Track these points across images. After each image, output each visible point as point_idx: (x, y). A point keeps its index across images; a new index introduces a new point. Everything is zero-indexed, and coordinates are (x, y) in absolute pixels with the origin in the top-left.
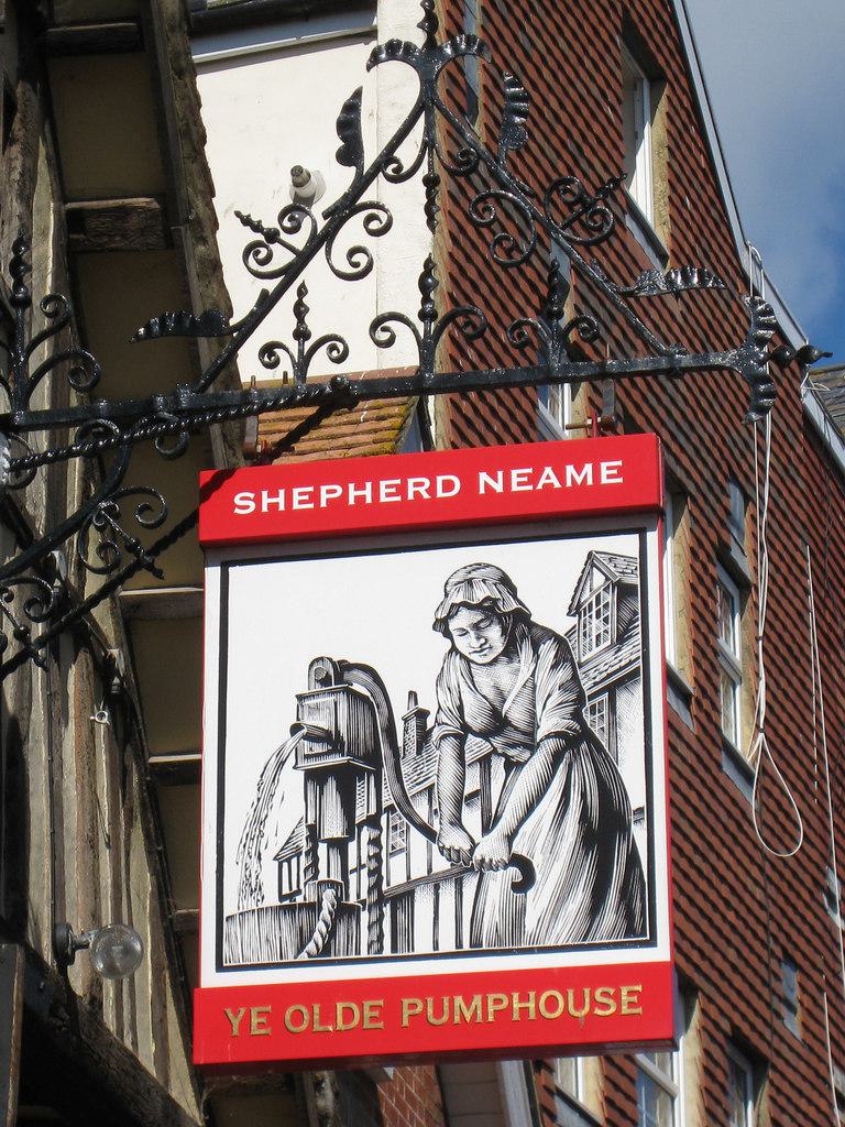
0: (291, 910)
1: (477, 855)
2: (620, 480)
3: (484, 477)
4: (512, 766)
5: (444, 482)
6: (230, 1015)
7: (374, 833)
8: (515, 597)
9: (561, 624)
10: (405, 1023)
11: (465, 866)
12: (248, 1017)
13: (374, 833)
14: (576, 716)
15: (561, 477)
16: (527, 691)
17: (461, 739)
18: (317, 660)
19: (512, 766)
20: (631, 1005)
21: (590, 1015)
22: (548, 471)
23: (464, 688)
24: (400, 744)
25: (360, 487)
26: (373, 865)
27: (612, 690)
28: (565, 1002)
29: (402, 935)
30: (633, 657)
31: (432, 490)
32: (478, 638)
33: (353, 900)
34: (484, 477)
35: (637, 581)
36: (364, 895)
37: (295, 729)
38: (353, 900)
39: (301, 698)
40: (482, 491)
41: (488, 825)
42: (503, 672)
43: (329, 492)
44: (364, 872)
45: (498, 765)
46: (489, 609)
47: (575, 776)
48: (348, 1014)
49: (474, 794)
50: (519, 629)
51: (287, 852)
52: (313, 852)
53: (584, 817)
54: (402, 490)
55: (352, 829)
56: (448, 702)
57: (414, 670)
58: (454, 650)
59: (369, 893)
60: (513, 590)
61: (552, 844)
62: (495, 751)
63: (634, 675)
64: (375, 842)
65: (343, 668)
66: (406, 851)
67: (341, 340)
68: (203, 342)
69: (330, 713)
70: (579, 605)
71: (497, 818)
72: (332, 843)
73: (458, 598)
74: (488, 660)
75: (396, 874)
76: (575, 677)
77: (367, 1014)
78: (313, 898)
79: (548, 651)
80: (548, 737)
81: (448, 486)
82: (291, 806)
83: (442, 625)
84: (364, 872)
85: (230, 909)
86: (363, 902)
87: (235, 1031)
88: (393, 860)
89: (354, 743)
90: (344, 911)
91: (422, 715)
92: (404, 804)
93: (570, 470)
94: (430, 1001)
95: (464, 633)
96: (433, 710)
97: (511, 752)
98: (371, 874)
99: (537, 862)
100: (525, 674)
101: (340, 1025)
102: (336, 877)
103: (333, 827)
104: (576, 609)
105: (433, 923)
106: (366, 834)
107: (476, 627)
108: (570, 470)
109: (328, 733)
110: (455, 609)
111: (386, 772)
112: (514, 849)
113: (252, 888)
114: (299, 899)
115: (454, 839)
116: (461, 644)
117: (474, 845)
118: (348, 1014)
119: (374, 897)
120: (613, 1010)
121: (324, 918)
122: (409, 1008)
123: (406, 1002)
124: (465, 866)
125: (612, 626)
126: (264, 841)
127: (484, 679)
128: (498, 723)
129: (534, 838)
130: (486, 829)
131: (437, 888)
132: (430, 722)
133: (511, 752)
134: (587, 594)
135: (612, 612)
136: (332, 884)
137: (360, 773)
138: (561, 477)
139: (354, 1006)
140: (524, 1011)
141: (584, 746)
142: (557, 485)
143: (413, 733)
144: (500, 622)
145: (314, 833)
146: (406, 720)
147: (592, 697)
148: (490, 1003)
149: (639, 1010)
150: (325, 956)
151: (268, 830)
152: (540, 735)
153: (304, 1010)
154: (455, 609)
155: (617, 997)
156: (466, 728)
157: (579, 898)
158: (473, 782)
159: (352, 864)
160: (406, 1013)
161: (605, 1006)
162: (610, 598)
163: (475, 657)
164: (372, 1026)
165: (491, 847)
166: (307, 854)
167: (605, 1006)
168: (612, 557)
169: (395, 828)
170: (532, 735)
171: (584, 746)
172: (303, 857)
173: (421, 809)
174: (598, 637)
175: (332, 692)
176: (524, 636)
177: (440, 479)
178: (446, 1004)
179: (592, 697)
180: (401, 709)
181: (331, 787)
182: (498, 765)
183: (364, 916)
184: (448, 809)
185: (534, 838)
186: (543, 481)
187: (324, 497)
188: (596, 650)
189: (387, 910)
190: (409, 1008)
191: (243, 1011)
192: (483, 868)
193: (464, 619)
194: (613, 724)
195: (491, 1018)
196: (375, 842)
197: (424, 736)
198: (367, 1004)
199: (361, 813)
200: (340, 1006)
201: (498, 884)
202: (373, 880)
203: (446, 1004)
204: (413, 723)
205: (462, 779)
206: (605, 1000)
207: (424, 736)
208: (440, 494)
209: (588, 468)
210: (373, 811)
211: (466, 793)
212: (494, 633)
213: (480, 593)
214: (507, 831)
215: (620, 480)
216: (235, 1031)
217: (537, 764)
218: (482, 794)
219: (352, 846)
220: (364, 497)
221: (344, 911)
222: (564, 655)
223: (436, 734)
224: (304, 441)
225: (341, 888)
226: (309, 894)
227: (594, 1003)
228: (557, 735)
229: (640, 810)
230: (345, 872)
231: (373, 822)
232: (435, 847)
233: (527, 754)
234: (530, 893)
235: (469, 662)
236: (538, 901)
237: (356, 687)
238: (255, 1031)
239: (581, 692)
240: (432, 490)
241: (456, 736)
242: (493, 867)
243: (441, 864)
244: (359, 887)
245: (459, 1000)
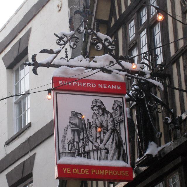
0: (71, 153)
1: (100, 147)
2: (120, 89)
3: (99, 85)
4: (105, 133)
5: (93, 85)
6: (64, 170)
7: (83, 142)
8: (103, 105)
9: (111, 111)
10: (92, 174)
11: (98, 149)
12: (67, 170)
13: (83, 142)
14: (114, 126)
15: (111, 86)
16: (106, 121)
17: (96, 128)
18: (72, 111)
19: (105, 133)
20: (69, 172)
21: (121, 175)
22: (109, 85)
23: (96, 119)
24: (87, 127)
25: (79, 83)
26: (83, 147)
27: (120, 122)
28: (117, 173)
31: (91, 85)
32: (98, 111)
33: (80, 152)
35: (122, 106)
36: (82, 152)
37: (69, 122)
38: (80, 152)
39: (70, 117)
40: (99, 87)
41: (101, 142)
42: (102, 117)
43: (75, 83)
44: (82, 148)
45: (102, 133)
46: (99, 107)
47: (114, 136)
48: (83, 172)
49: (99, 137)
50: (105, 111)
51: (69, 143)
52: (73, 143)
53: (116, 143)
54: (86, 85)
55: (80, 140)
56: (94, 122)
57: (87, 115)
58: (94, 113)
59: (83, 151)
60: (103, 104)
62: (101, 130)
63: (122, 121)
64: (83, 143)
65: (77, 113)
66: (88, 145)
67: (57, 43)
69: (75, 121)
70: (114, 108)
71: (103, 141)
72: (77, 142)
73: (95, 104)
74: (100, 115)
75: (87, 149)
76: (113, 120)
77: (86, 171)
78: (74, 151)
79: (109, 115)
80: (110, 129)
81: (94, 85)
83: (92, 108)
84: (82, 148)
85: (61, 152)
86: (82, 153)
87: (65, 172)
88: (87, 146)
89: (79, 126)
91: (90, 123)
92: (88, 137)
93: (113, 86)
94: (96, 170)
95: (96, 110)
96: (92, 122)
97: (104, 131)
98: (83, 148)
99: (109, 149)
100: (106, 118)
101: (82, 173)
102: (77, 148)
103: (77, 140)
104: (113, 109)
106: (82, 141)
107: (98, 109)
108: (113, 86)
109: (75, 124)
110: (94, 106)
111: (85, 132)
112: (106, 147)
113: (64, 148)
114: (72, 151)
115: (96, 144)
116: (95, 112)
117: (99, 146)
118: (83, 172)
119: (84, 152)
120: (124, 175)
122: (93, 171)
123: (92, 170)
124: (98, 149)
125: (119, 113)
126: (65, 141)
127: (99, 118)
128: (102, 126)
129: (109, 145)
130: (101, 143)
131: (94, 152)
132: (91, 124)
133: (104, 131)
134: (115, 107)
135: (119, 110)
136: (77, 149)
137: (80, 131)
138: (111, 86)
139: (84, 170)
140: (111, 173)
141: (115, 131)
142: (111, 88)
143: (89, 126)
144: (101, 109)
145: (74, 140)
146: (87, 123)
147: (116, 124)
148: (86, 171)
149: (70, 173)
151: (66, 139)
152: (109, 129)
153: (76, 170)
154: (94, 106)
155: (125, 173)
156: (97, 126)
158: (98, 135)
159: (80, 146)
160: (92, 172)
161: (123, 174)
162: (118, 108)
163: (98, 114)
164: (127, 175)
165: (102, 146)
166: (73, 144)
167: (123, 174)
168: (118, 101)
169: (86, 141)
170: (108, 128)
171: (115, 131)
172: (72, 144)
173: (91, 139)
174: (117, 114)
175: (75, 117)
176: (105, 112)
177: (92, 84)
178: (99, 171)
179: (116, 124)
180: (86, 121)
181: (76, 133)
182: (102, 133)
183: (83, 155)
184: (95, 139)
185: (109, 145)
186: (109, 87)
187: (74, 84)
188: (117, 116)
189: (86, 154)
190: (93, 171)
191: (66, 169)
192: (101, 149)
193: (95, 108)
194: (120, 128)
195: (106, 174)
196: (83, 143)
197: (90, 127)
198: (86, 170)
199: (81, 138)
200: (82, 170)
202: (83, 149)
203: (99, 171)
204: (88, 124)
205: (97, 134)
206: (123, 173)
207: (90, 127)
208: (92, 86)
209: (115, 86)
210: (83, 138)
211: (97, 137)
212: (100, 111)
213: (98, 104)
214: (104, 144)
215: (120, 89)
216: (65, 172)
217: (108, 134)
218: (100, 137)
219: (80, 143)
220: (80, 85)
222: (111, 116)
223: (92, 126)
225: (78, 150)
226: (73, 151)
227: (122, 173)
228: (111, 129)
229: (124, 143)
230: (79, 148)
231: (83, 139)
232: (93, 145)
233: (107, 132)
234: (109, 154)
235: (97, 115)
237: (79, 117)
238: (68, 172)
239: (115, 123)
240: (91, 85)
241: (95, 127)
242: (103, 150)
243: (94, 148)
244: (81, 150)
245: (100, 171)
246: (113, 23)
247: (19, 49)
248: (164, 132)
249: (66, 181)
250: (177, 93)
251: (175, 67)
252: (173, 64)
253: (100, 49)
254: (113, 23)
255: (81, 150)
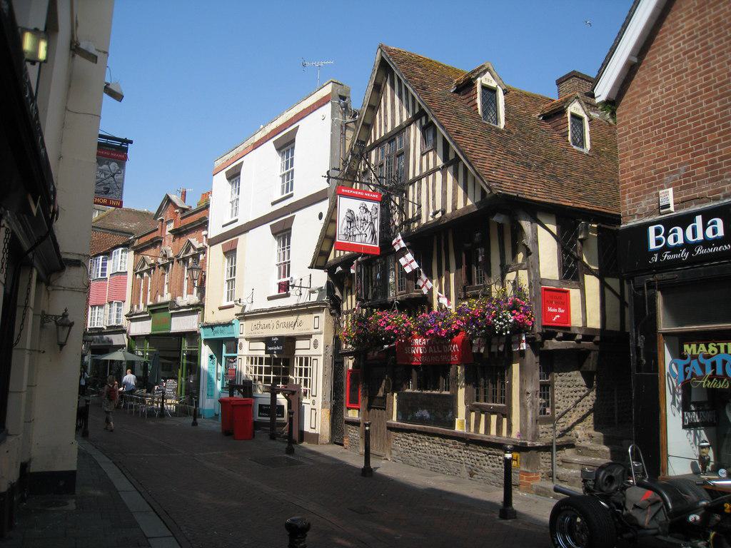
3: (686, 347)
11: (361, 234)
27: (375, 218)
29: (355, 239)
30: (562, 420)
34: (686, 347)
46: (364, 207)
57: (357, 213)
61: (369, 233)
68: (398, 363)
69: (349, 215)
75: (355, 234)
82: (345, 224)
90: (350, 236)
105: (358, 239)
121: (348, 236)
124: (361, 234)
128: (364, 220)
150: (348, 240)
157: (371, 239)
165: (363, 232)
201: (364, 236)
221: (350, 236)
224: (662, 33)
236: (367, 238)
244: (351, 234)
246: (369, 144)
247: (68, 334)
248: (328, 215)
249: (101, 136)
250: (410, 204)
251: (411, 187)
252: (410, 185)
253: (597, 100)
254: (369, 144)
255: (351, 234)
